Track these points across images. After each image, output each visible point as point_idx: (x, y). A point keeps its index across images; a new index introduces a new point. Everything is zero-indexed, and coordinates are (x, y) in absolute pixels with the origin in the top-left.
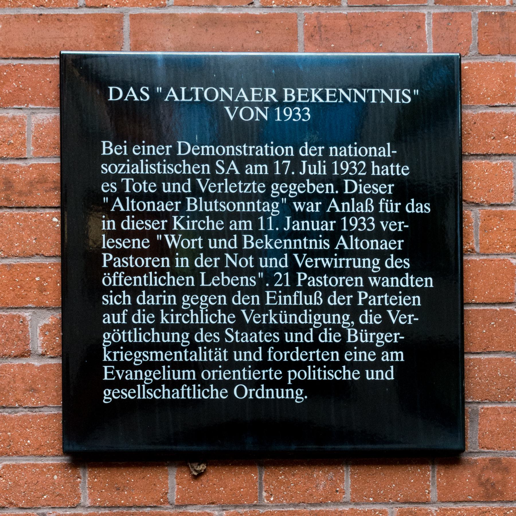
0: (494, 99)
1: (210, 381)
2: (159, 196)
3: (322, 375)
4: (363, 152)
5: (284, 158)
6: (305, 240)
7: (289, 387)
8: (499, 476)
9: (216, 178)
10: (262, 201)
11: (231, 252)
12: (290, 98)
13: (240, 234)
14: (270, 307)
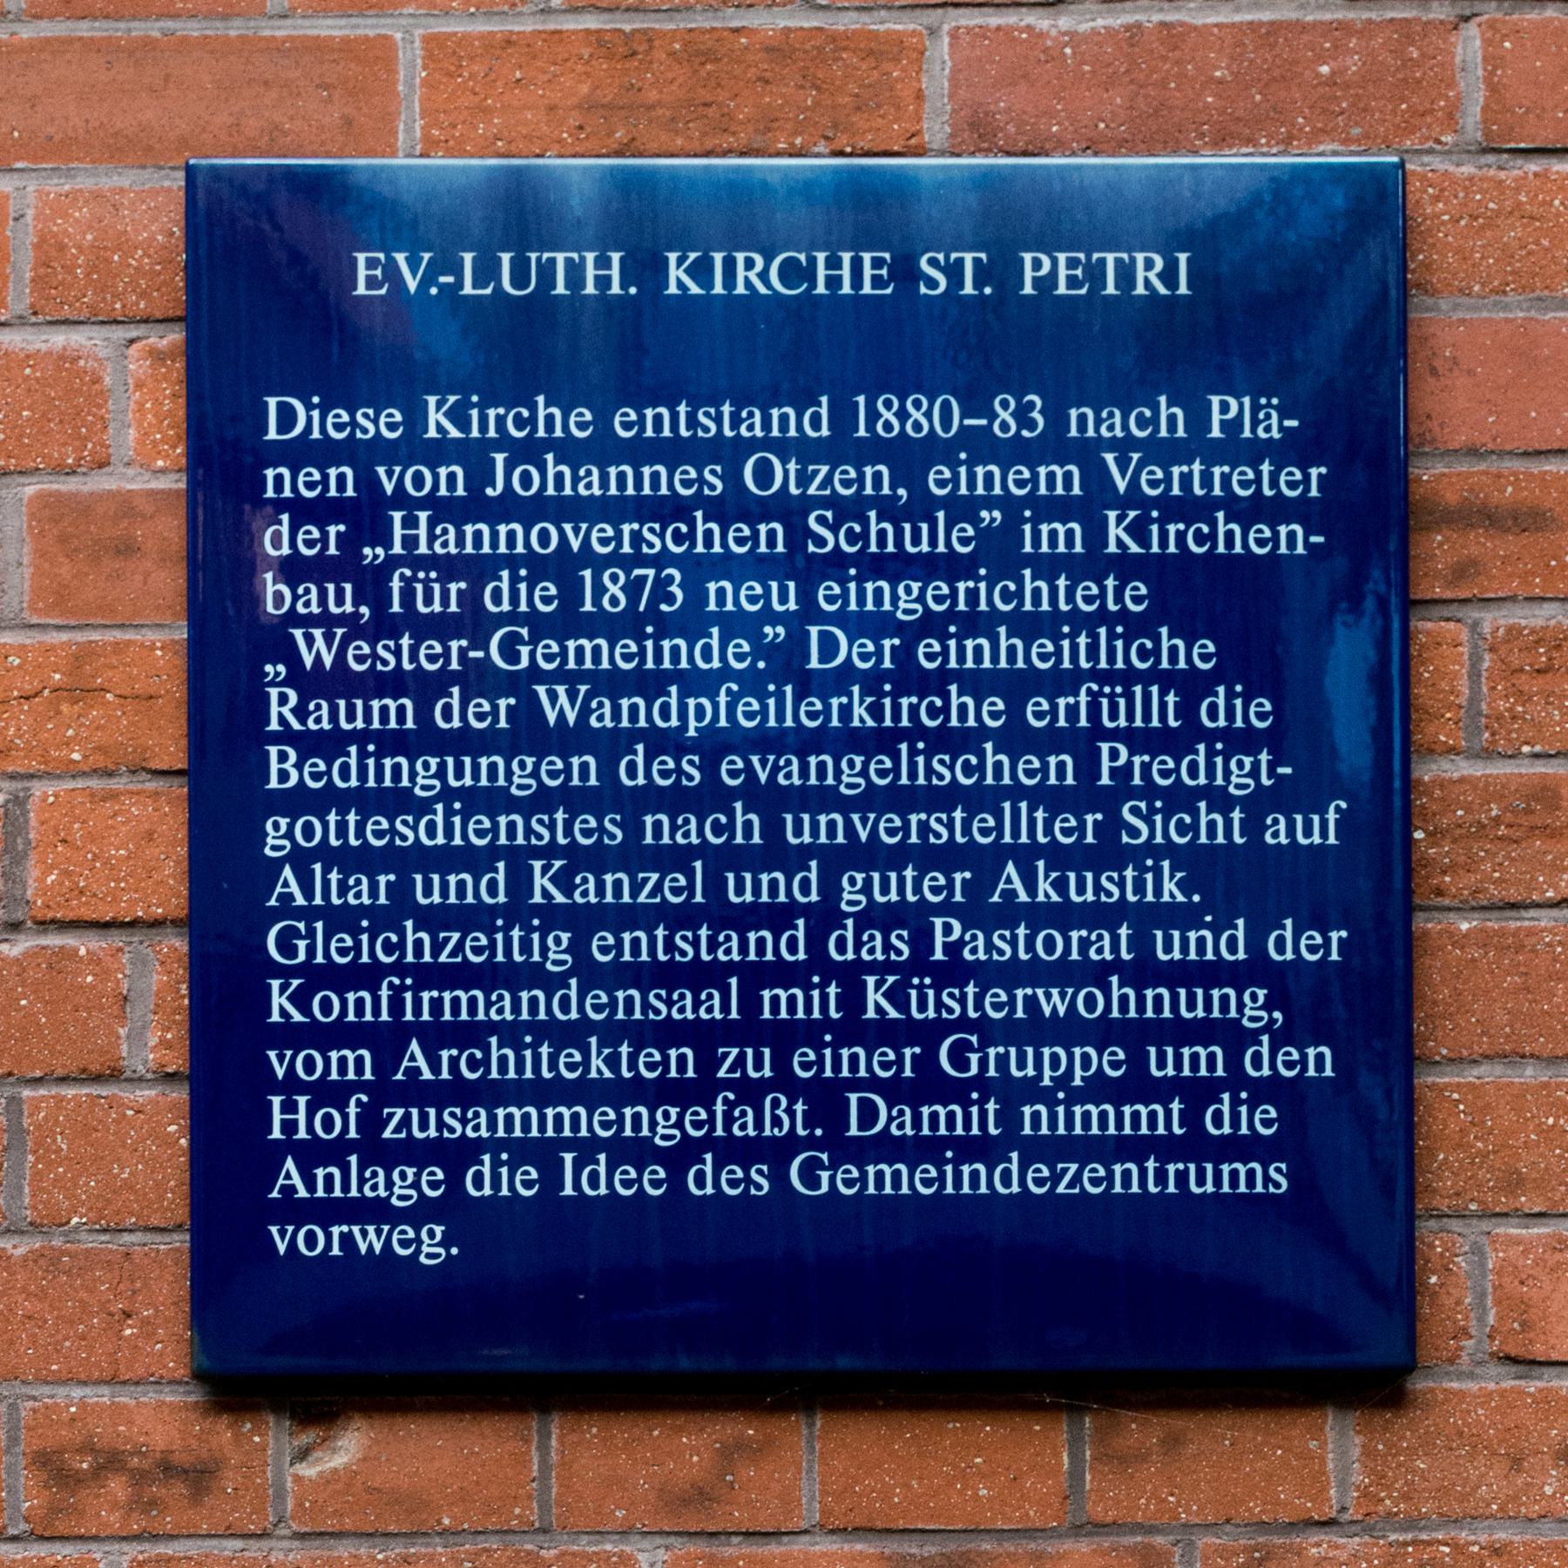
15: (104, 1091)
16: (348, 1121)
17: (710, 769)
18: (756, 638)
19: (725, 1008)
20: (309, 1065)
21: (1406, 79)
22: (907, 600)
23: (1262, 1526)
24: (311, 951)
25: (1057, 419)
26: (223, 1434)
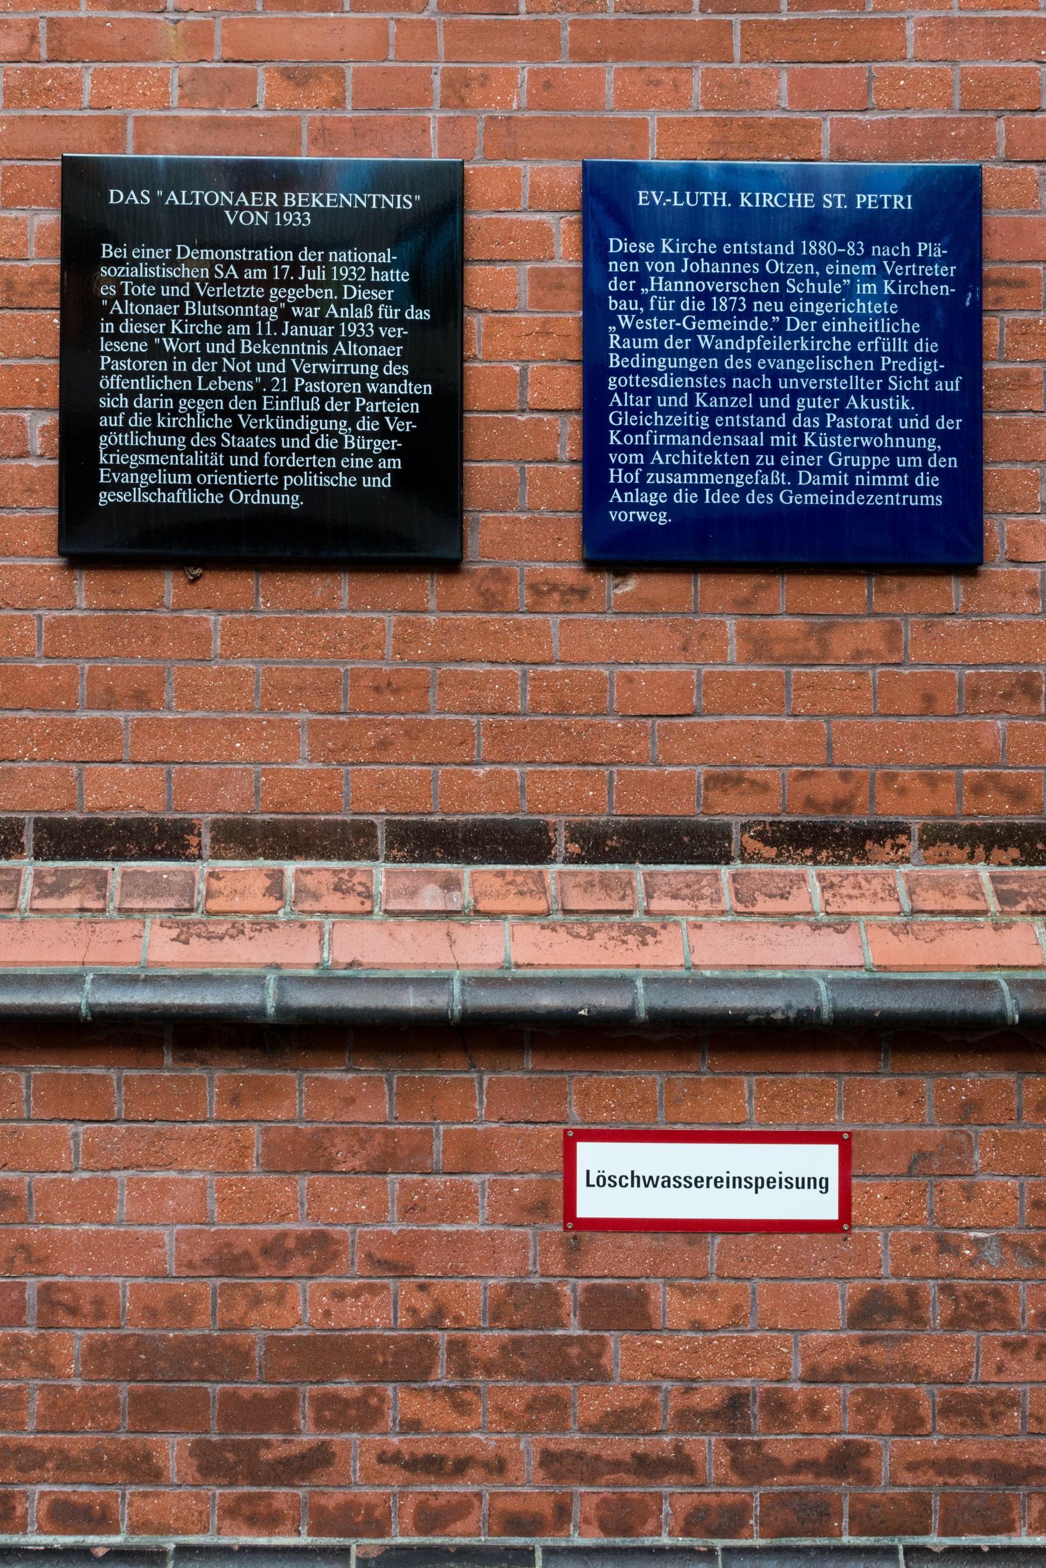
0: (499, 205)
1: (206, 486)
4: (363, 257)
5: (283, 262)
7: (285, 492)
8: (499, 586)
9: (215, 282)
10: (261, 305)
11: (229, 357)
12: (290, 203)
13: (238, 339)
14: (267, 412)
16: (635, 477)
17: (754, 364)
18: (770, 321)
20: (623, 459)
21: (983, 139)
22: (819, 309)
23: (931, 615)
25: (868, 251)
26: (591, 579)
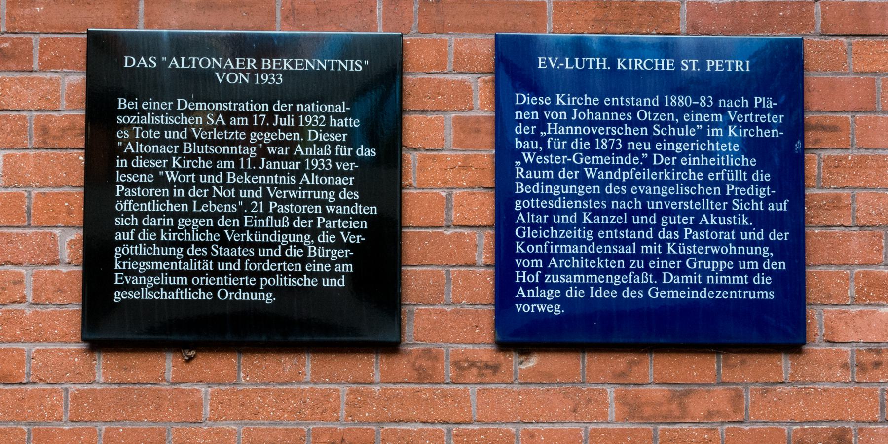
1: (199, 286)
2: (162, 141)
3: (287, 282)
4: (323, 108)
5: (261, 112)
6: (276, 176)
7: (261, 291)
11: (218, 185)
13: (225, 171)
14: (247, 228)
15: (471, 269)
16: (536, 278)
17: (628, 190)
19: (632, 250)
21: (802, 15)
23: (766, 384)
24: (527, 234)
26: (501, 357)
